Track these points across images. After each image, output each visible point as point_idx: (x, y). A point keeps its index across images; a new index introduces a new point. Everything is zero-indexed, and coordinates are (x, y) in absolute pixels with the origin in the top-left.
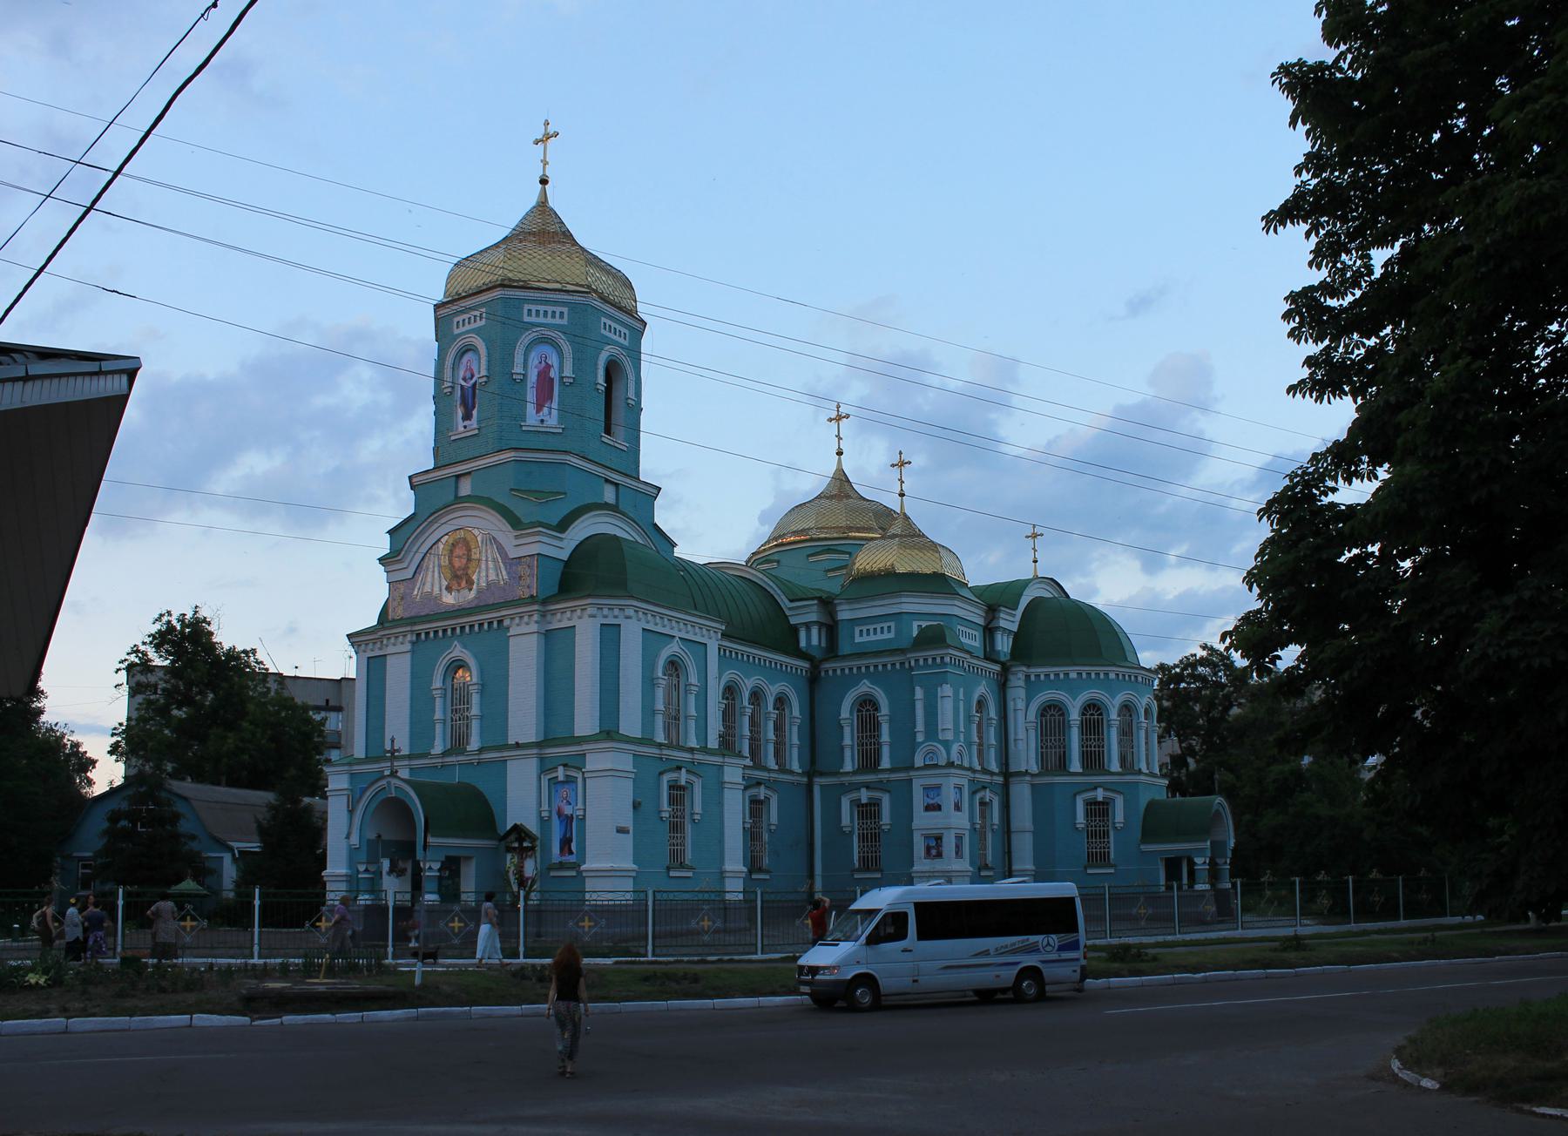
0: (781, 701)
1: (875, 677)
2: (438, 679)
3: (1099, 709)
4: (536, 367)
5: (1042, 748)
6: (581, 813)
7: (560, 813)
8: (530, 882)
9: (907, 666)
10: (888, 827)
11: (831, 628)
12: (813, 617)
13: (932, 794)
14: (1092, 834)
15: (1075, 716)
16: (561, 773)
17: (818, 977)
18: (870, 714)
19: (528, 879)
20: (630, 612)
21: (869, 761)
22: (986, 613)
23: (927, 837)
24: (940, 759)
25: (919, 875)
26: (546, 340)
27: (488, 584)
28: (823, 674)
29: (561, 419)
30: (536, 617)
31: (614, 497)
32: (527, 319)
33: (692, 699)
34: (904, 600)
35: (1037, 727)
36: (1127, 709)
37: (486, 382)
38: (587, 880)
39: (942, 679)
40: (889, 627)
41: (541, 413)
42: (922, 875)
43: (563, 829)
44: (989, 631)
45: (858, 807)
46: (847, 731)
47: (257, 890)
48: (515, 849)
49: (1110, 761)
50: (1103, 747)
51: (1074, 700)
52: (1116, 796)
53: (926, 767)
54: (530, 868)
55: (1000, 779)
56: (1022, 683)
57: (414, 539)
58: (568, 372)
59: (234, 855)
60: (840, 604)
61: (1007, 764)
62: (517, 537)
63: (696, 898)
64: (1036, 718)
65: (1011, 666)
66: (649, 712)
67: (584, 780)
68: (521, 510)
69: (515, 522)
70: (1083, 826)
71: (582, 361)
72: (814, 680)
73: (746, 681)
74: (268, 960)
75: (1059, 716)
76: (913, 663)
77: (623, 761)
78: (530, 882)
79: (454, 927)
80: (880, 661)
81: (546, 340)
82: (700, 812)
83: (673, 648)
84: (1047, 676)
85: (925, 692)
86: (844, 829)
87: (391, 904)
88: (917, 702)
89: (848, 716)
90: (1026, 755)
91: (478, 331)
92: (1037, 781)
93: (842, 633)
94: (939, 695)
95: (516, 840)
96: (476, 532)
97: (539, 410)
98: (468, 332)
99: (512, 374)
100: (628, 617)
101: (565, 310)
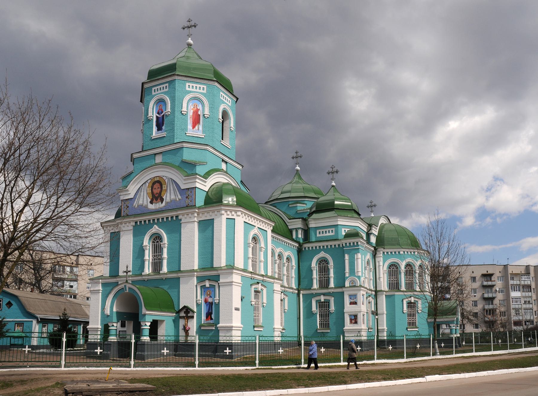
0: (288, 259)
1: (326, 250)
3: (326, 261)
4: (192, 109)
5: (389, 281)
6: (218, 301)
9: (341, 246)
11: (306, 232)
12: (300, 226)
13: (352, 298)
14: (409, 315)
20: (239, 213)
21: (324, 283)
22: (368, 227)
23: (350, 315)
24: (356, 283)
25: (347, 331)
26: (197, 98)
27: (171, 201)
28: (303, 249)
29: (204, 132)
31: (225, 168)
32: (187, 89)
33: (262, 253)
35: (387, 273)
36: (409, 265)
38: (220, 331)
39: (357, 250)
40: (332, 231)
41: (195, 129)
43: (208, 307)
44: (368, 235)
45: (319, 303)
46: (315, 273)
47: (65, 334)
55: (374, 293)
56: (381, 255)
57: (134, 181)
58: (207, 112)
59: (38, 320)
61: (376, 287)
62: (185, 180)
64: (387, 269)
66: (246, 258)
67: (219, 286)
70: (406, 312)
71: (213, 107)
72: (300, 251)
73: (276, 249)
76: (344, 245)
81: (197, 98)
82: (266, 303)
83: (255, 231)
87: (257, 342)
89: (315, 265)
90: (384, 285)
96: (164, 178)
99: (182, 111)
101: (167, 85)
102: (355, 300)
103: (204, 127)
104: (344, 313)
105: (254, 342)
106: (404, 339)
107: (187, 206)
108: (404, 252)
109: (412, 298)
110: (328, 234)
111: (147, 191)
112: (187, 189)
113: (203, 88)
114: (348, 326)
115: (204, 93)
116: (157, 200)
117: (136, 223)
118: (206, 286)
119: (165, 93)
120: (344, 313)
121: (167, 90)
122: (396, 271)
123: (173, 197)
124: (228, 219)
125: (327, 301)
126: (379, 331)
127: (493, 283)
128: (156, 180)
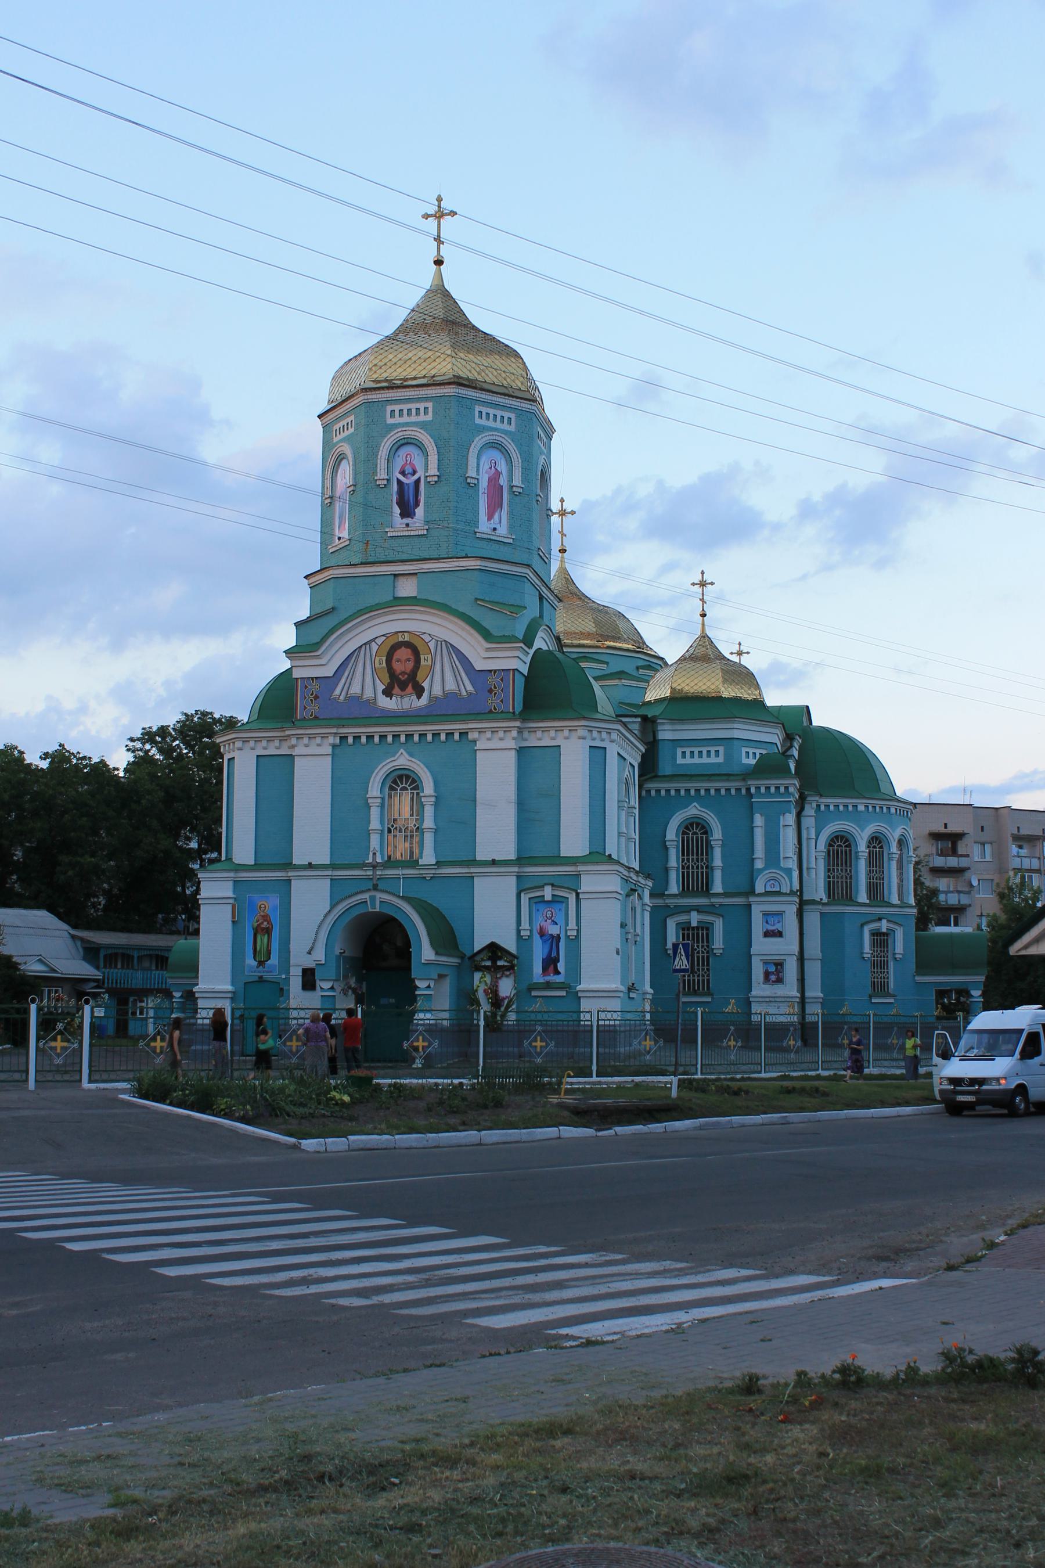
2: (376, 785)
7: (542, 933)
8: (506, 1002)
10: (721, 951)
13: (771, 920)
15: (862, 847)
16: (548, 893)
17: (984, 1087)
18: (688, 838)
19: (504, 999)
23: (766, 963)
25: (757, 999)
29: (511, 527)
30: (514, 733)
32: (478, 421)
34: (736, 726)
36: (877, 841)
37: (436, 482)
38: (582, 1000)
40: (717, 752)
42: (760, 1000)
45: (683, 929)
48: (487, 968)
49: (890, 893)
50: (883, 879)
51: (894, 831)
52: (896, 927)
53: (767, 893)
54: (506, 987)
56: (812, 813)
58: (517, 481)
60: (663, 723)
62: (488, 650)
63: (528, 1019)
64: (677, 836)
65: (808, 795)
68: (489, 622)
69: (486, 635)
70: (869, 956)
74: (398, 1081)
75: (846, 846)
77: (612, 883)
78: (506, 1002)
79: (155, 1047)
80: (713, 785)
84: (837, 806)
85: (765, 820)
86: (715, 951)
88: (756, 830)
89: (674, 838)
91: (423, 425)
92: (827, 909)
93: (663, 753)
94: (781, 823)
95: (489, 959)
96: (427, 638)
97: (490, 517)
98: (415, 424)
100: (612, 741)
101: (430, 405)
102: (778, 927)
103: (511, 514)
104: (750, 957)
105: (588, 1025)
106: (818, 1022)
107: (491, 712)
108: (867, 807)
109: (884, 922)
110: (705, 760)
111: (373, 663)
112: (490, 671)
113: (510, 419)
114: (760, 989)
115: (510, 432)
116: (403, 687)
117: (343, 738)
118: (546, 899)
119: (423, 425)
120: (750, 956)
121: (429, 417)
122: (846, 852)
123: (451, 686)
124: (592, 750)
125: (703, 925)
126: (807, 1000)
127: (964, 862)
128: (400, 639)
